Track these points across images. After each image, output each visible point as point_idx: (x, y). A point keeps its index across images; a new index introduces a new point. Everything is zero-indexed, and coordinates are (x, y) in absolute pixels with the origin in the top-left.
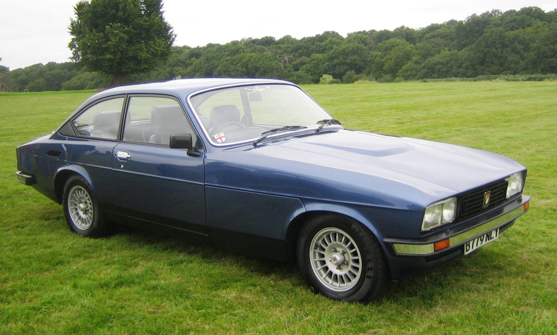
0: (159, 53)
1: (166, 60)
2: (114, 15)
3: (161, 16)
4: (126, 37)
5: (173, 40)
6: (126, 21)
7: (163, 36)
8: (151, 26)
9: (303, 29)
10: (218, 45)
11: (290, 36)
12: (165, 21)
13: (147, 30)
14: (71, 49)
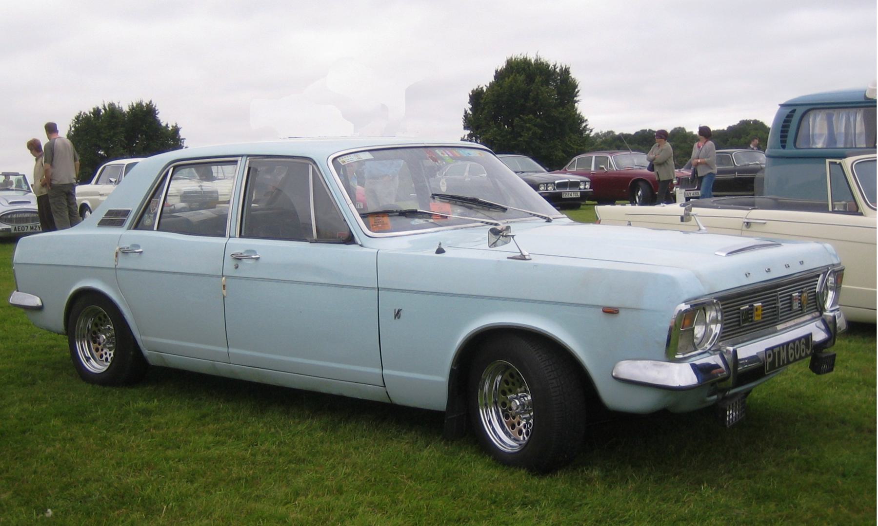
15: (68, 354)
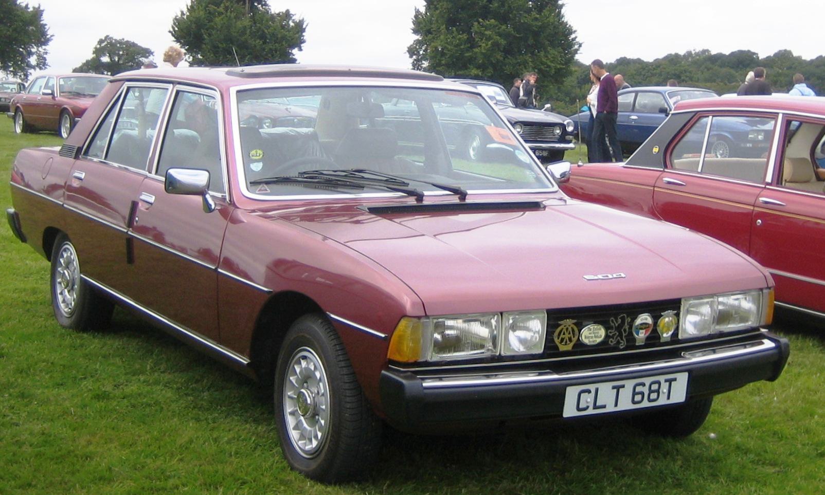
0: (553, 71)
1: (562, 83)
2: (485, 7)
3: (560, 12)
4: (503, 42)
5: (576, 51)
6: (503, 19)
7: (561, 45)
8: (543, 28)
9: (724, 46)
10: (639, 61)
11: (790, 53)
12: (565, 20)
13: (536, 34)
14: (411, 57)
15: (49, 296)
